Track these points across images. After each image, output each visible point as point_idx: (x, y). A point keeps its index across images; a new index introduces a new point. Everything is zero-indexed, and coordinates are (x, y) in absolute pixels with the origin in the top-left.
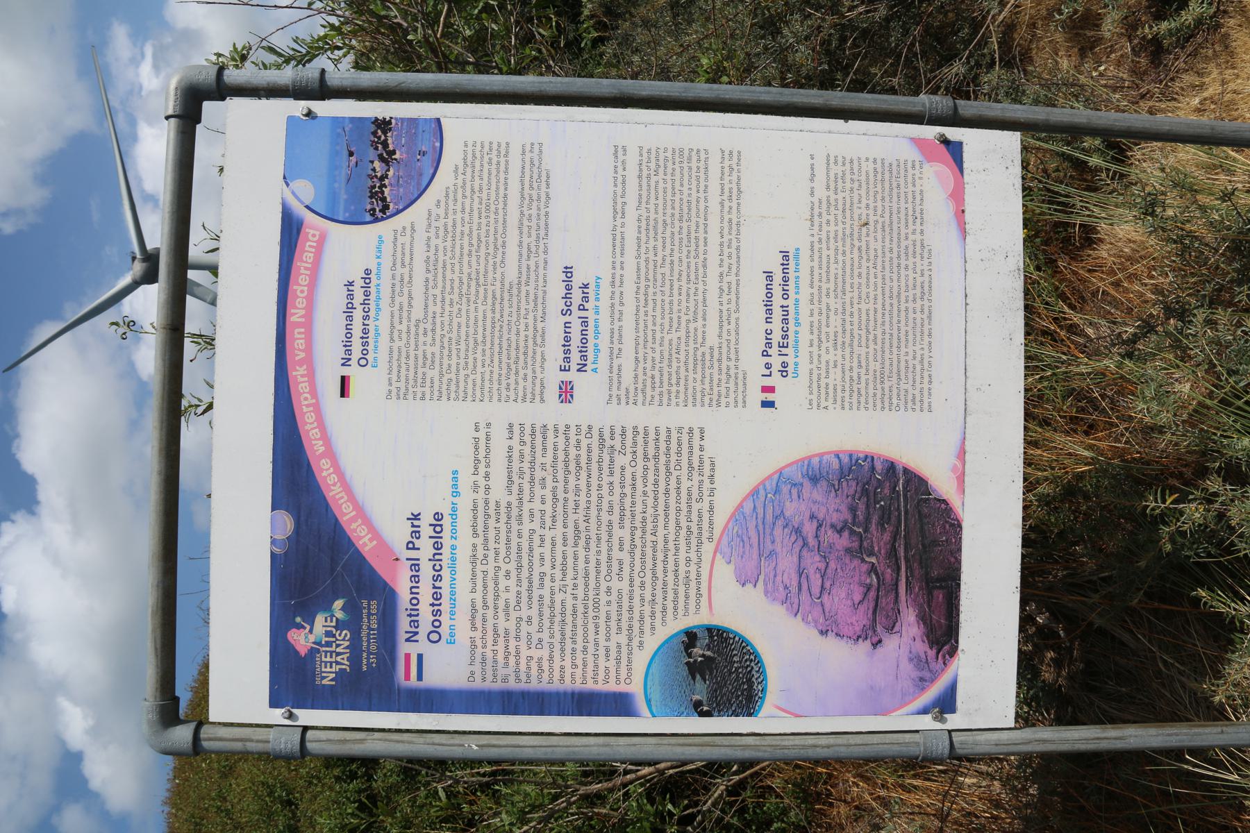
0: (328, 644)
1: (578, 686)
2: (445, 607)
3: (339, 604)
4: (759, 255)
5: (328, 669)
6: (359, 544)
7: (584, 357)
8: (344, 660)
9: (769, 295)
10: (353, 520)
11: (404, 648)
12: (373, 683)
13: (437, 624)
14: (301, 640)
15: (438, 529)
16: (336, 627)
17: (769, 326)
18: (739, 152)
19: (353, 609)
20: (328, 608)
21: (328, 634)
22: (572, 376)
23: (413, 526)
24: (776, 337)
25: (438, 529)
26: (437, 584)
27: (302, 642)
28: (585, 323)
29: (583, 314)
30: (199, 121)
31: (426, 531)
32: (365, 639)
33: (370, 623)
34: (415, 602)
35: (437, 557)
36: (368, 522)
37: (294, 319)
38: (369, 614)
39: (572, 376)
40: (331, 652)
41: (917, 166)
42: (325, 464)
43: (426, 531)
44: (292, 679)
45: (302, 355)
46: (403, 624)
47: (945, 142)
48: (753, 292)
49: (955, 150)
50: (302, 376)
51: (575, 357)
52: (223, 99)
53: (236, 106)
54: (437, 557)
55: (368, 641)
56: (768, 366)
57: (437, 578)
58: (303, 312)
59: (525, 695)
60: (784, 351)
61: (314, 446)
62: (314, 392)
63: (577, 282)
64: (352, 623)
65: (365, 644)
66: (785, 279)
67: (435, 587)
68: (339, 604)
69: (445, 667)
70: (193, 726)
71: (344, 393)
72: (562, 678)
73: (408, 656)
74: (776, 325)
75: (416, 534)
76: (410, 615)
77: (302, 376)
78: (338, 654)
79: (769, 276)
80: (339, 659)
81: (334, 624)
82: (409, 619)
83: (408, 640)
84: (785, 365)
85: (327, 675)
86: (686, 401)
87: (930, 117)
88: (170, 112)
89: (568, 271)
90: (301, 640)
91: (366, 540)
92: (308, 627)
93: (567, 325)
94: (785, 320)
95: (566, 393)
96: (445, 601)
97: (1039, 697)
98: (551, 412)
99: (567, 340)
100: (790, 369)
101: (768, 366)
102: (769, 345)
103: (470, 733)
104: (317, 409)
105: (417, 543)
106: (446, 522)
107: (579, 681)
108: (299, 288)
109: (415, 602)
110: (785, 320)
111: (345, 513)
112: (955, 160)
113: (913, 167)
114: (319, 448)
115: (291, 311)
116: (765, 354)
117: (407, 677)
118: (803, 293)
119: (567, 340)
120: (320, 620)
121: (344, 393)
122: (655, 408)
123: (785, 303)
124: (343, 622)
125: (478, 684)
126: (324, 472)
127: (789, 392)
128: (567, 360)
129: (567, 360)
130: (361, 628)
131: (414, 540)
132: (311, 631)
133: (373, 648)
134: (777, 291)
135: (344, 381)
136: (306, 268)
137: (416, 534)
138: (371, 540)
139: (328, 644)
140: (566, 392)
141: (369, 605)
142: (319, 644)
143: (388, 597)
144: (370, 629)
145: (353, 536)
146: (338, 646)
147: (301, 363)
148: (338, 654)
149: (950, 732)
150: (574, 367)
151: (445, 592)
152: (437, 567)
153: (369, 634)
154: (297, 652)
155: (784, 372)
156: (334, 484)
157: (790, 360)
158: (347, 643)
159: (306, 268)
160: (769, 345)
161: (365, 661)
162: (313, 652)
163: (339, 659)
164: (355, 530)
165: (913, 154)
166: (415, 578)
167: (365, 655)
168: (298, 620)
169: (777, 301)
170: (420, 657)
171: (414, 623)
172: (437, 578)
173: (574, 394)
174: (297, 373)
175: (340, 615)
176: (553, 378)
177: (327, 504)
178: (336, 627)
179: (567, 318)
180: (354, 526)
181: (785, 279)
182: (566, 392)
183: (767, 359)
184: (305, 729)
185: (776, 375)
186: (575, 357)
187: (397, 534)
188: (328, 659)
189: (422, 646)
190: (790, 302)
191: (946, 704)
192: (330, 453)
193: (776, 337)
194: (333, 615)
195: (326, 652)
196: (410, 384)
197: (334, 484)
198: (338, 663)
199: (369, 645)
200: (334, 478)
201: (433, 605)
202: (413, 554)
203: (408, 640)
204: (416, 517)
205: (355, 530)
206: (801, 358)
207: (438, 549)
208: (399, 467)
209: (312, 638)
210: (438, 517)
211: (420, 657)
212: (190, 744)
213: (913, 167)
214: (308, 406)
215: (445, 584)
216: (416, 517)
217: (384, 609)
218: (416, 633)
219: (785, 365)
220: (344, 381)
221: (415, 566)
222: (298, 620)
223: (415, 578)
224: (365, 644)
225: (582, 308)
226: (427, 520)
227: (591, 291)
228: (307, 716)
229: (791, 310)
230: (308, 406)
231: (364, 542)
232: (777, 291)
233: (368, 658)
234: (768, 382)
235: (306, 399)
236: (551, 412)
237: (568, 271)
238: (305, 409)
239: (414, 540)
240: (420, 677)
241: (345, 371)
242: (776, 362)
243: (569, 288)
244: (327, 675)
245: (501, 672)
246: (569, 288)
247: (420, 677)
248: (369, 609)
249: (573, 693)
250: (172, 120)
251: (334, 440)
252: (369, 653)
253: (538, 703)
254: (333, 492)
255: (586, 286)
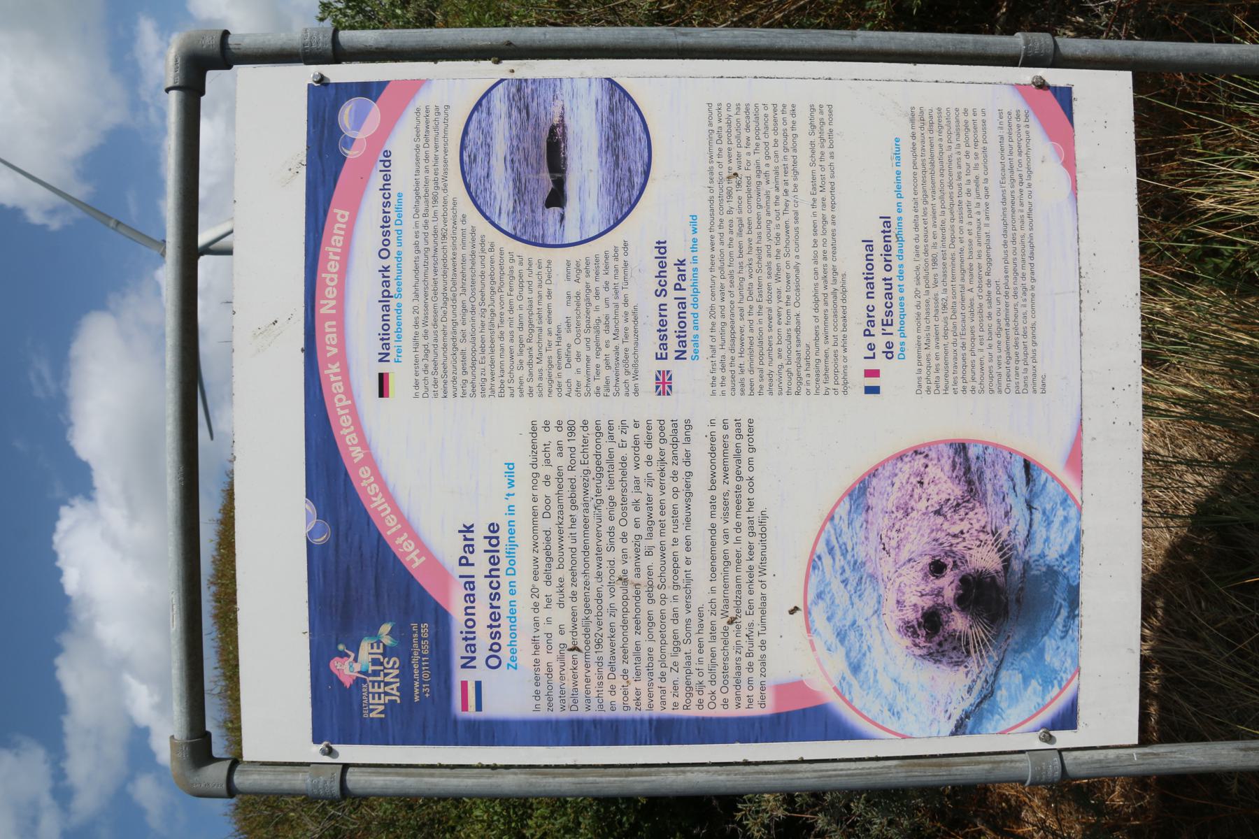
0: (376, 673)
1: (657, 711)
2: (505, 630)
3: (386, 628)
4: (858, 222)
5: (376, 701)
6: (406, 560)
7: (683, 343)
8: (394, 689)
9: (870, 266)
10: (398, 534)
11: (460, 675)
12: (429, 713)
13: (496, 647)
14: (346, 669)
15: (494, 542)
16: (384, 655)
17: (871, 302)
18: (793, 106)
19: (403, 635)
20: (373, 632)
21: (375, 662)
22: (670, 364)
23: (466, 539)
24: (879, 315)
25: (494, 542)
26: (495, 603)
27: (347, 672)
28: (682, 304)
29: (680, 294)
30: (202, 93)
31: (481, 544)
32: (416, 666)
33: (421, 650)
34: (470, 623)
35: (494, 573)
36: (415, 537)
37: (323, 311)
38: (420, 639)
39: (670, 364)
40: (379, 682)
41: (1023, 118)
42: (365, 472)
43: (481, 544)
44: (336, 712)
45: (335, 351)
46: (459, 649)
47: (1042, 85)
48: (851, 262)
49: (1064, 97)
50: (335, 375)
51: (673, 343)
52: (229, 67)
53: (243, 73)
54: (494, 573)
55: (420, 668)
56: (871, 347)
57: (495, 596)
58: (334, 303)
59: (596, 723)
60: (889, 329)
61: (352, 453)
62: (349, 393)
63: (671, 259)
64: (402, 649)
65: (416, 672)
66: (888, 249)
67: (492, 607)
68: (386, 628)
69: (507, 696)
70: (226, 764)
71: (383, 392)
72: (651, 707)
73: (464, 684)
74: (879, 301)
75: (469, 547)
76: (466, 639)
77: (335, 375)
78: (387, 684)
79: (869, 245)
80: (387, 689)
81: (381, 651)
82: (465, 643)
83: (464, 666)
84: (889, 345)
85: (375, 707)
86: (733, 389)
87: (1026, 57)
88: (170, 84)
89: (661, 246)
90: (346, 669)
91: (413, 556)
92: (353, 655)
93: (662, 308)
94: (889, 295)
95: (664, 384)
96: (504, 622)
97: (1165, 713)
98: (649, 406)
99: (663, 323)
100: (896, 350)
101: (871, 347)
102: (871, 323)
103: (389, 766)
104: (353, 411)
105: (471, 558)
106: (503, 534)
107: (644, 706)
108: (328, 276)
109: (470, 623)
110: (889, 295)
111: (389, 526)
112: (1064, 109)
113: (1018, 117)
114: (357, 454)
115: (320, 302)
116: (867, 333)
117: (465, 707)
118: (908, 261)
119: (663, 323)
120: (365, 646)
121: (383, 392)
122: (746, 396)
123: (888, 275)
124: (391, 648)
125: (543, 714)
126: (363, 479)
127: (894, 374)
128: (664, 346)
129: (664, 346)
130: (411, 654)
131: (468, 555)
132: (356, 660)
133: (426, 676)
134: (879, 263)
135: (383, 379)
136: (335, 254)
137: (469, 547)
138: (419, 556)
139: (376, 673)
140: (664, 383)
141: (419, 628)
142: (365, 673)
143: (441, 618)
144: (421, 655)
145: (398, 552)
146: (386, 675)
147: (333, 360)
148: (387, 684)
149: (1060, 751)
150: (672, 355)
151: (504, 611)
152: (495, 585)
153: (420, 661)
154: (341, 683)
155: (889, 354)
156: (376, 495)
157: (895, 339)
158: (397, 672)
159: (335, 254)
160: (871, 323)
161: (417, 691)
162: (358, 682)
163: (387, 689)
164: (401, 546)
165: (1014, 103)
166: (470, 597)
167: (417, 684)
168: (341, 647)
169: (879, 273)
170: (478, 685)
171: (471, 647)
172: (495, 596)
173: (673, 385)
174: (330, 372)
175: (388, 641)
176: (649, 367)
177: (369, 518)
178: (384, 655)
179: (662, 300)
180: (399, 541)
181: (888, 249)
182: (664, 383)
183: (870, 339)
184: (346, 767)
185: (880, 357)
186: (673, 343)
187: (447, 548)
188: (376, 690)
189: (480, 672)
190: (893, 274)
191: (1068, 718)
192: (370, 460)
193: (879, 315)
194: (379, 642)
195: (373, 682)
196: (434, 382)
197: (376, 495)
198: (386, 694)
199: (420, 674)
200: (374, 489)
201: (491, 626)
202: (467, 570)
203: (464, 666)
204: (469, 529)
205: (401, 546)
206: (909, 335)
207: (494, 564)
208: (443, 475)
209: (357, 667)
210: (494, 528)
211: (478, 685)
212: (224, 786)
213: (1018, 117)
214: (343, 408)
215: (504, 603)
216: (469, 529)
217: (436, 633)
218: (473, 658)
219: (889, 345)
220: (383, 379)
221: (470, 584)
222: (341, 647)
223: (470, 597)
224: (416, 672)
225: (678, 288)
226: (481, 531)
227: (688, 268)
228: (348, 753)
229: (895, 282)
230: (343, 408)
231: (413, 560)
232: (879, 263)
233: (420, 688)
234: (871, 365)
235: (340, 400)
236: (649, 406)
237: (661, 246)
238: (340, 412)
239: (468, 555)
240: (479, 707)
241: (384, 368)
242: (880, 342)
243: (663, 266)
244: (375, 707)
245: (607, 698)
246: (663, 266)
247: (479, 707)
248: (420, 633)
249: (651, 720)
250: (173, 93)
251: (373, 445)
252: (422, 682)
253: (664, 731)
254: (376, 504)
255: (682, 263)
